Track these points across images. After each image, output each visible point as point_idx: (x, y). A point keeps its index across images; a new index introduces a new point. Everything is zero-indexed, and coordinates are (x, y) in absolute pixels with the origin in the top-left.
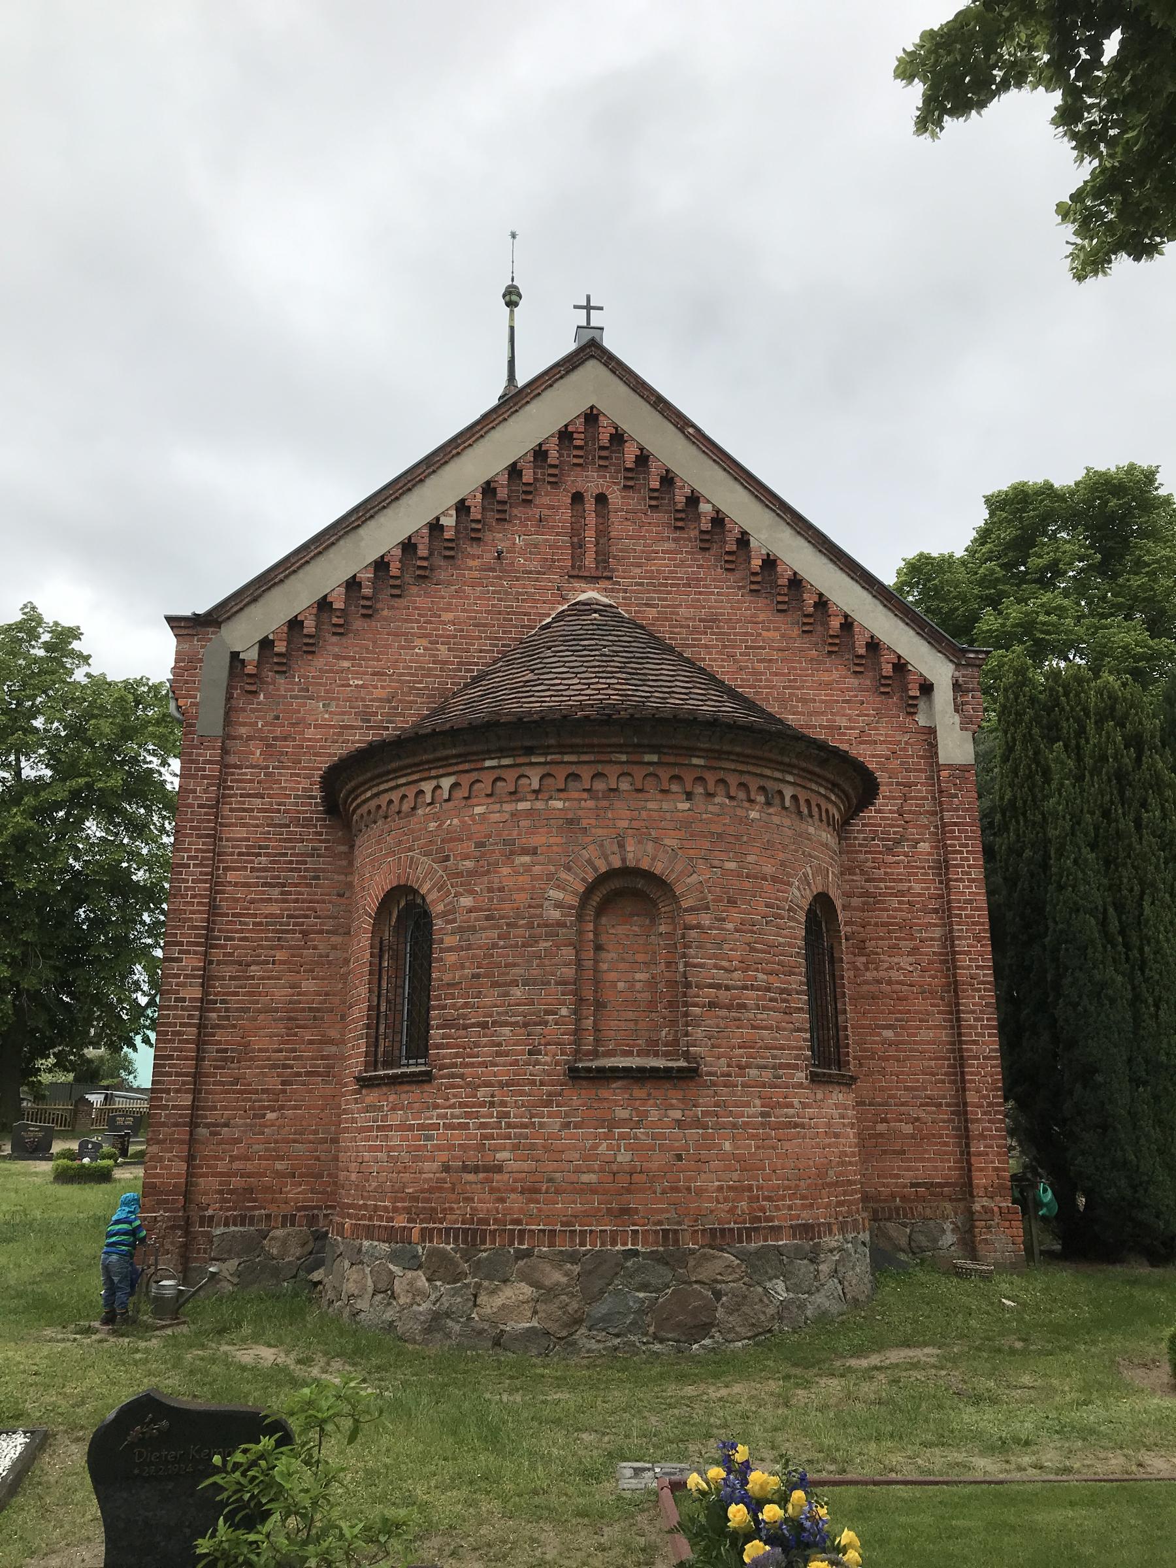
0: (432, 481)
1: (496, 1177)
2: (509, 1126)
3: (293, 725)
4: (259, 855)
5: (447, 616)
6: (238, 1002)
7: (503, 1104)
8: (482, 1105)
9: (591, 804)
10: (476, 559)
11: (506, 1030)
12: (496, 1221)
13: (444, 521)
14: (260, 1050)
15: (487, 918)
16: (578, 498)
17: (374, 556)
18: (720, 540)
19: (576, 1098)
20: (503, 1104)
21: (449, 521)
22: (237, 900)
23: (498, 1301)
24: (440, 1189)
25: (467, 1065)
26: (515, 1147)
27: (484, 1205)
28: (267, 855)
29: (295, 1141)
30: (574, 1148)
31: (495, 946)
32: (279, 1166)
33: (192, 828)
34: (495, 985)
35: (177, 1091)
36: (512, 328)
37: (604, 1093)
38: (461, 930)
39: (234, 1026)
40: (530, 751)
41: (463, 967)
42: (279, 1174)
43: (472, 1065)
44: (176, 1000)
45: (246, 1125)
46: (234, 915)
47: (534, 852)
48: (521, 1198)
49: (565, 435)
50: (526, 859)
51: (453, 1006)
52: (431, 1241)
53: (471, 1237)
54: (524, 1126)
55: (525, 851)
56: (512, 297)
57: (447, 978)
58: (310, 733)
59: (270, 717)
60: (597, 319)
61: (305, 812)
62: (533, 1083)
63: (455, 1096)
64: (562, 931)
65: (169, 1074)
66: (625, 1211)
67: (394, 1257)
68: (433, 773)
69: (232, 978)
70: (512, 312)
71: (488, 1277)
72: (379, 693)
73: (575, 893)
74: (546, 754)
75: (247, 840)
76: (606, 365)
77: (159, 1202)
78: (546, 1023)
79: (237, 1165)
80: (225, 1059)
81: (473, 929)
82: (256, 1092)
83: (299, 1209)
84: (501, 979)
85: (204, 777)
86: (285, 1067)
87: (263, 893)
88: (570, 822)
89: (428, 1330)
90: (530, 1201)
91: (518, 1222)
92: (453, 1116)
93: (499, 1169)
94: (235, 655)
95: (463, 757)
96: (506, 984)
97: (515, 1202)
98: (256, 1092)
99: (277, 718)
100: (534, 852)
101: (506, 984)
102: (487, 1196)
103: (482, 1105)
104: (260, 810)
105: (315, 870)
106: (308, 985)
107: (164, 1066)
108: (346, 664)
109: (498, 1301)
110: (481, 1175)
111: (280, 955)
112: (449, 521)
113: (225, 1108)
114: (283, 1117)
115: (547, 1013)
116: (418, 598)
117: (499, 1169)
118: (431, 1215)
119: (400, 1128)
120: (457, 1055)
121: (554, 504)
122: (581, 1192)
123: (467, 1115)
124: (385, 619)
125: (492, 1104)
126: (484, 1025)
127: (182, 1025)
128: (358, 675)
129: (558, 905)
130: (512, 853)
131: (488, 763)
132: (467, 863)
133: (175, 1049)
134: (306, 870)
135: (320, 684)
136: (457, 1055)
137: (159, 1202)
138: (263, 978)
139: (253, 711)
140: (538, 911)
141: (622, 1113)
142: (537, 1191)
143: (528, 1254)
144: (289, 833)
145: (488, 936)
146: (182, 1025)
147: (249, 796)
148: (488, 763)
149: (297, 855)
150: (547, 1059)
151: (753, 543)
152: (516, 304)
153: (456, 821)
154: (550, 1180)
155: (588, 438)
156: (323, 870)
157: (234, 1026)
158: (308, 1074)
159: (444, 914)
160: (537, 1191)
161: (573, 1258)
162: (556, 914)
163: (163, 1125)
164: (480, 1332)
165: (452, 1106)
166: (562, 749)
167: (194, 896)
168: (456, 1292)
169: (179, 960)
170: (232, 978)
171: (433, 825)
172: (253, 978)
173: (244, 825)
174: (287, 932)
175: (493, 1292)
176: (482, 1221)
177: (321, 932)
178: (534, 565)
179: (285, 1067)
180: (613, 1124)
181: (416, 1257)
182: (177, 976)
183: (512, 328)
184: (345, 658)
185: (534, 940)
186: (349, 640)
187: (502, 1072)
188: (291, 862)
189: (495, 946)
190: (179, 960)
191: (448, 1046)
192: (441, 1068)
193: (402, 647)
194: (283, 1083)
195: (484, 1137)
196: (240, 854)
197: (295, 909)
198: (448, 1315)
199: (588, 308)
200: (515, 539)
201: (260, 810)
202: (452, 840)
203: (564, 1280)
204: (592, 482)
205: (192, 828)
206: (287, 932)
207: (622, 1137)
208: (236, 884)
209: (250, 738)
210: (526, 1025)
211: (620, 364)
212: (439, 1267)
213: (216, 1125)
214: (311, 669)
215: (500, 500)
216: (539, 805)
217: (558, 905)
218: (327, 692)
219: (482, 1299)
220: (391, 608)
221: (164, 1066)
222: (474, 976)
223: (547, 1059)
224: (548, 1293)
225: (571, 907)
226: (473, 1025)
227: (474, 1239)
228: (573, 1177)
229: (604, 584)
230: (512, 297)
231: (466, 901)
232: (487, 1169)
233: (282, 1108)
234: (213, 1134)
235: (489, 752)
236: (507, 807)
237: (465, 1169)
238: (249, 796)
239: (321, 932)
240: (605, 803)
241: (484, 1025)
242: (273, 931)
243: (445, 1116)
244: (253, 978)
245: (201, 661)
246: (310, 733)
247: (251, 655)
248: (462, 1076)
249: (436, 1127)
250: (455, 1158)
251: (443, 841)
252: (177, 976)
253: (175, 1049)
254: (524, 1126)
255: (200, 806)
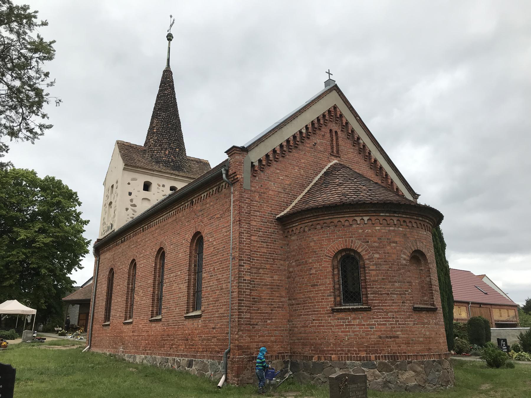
0: (299, 117)
1: (397, 339)
2: (399, 324)
3: (266, 189)
4: (259, 231)
5: (303, 161)
6: (257, 282)
7: (397, 318)
8: (390, 318)
9: (408, 230)
10: (308, 144)
11: (395, 296)
12: (399, 353)
13: (303, 131)
14: (264, 299)
15: (385, 261)
16: (331, 130)
17: (286, 138)
18: (363, 150)
19: (415, 316)
20: (397, 318)
21: (304, 131)
22: (255, 246)
23: (405, 377)
24: (378, 344)
25: (383, 306)
26: (402, 331)
27: (394, 348)
28: (262, 232)
29: (276, 330)
30: (416, 331)
31: (388, 270)
32: (273, 339)
33: (244, 220)
34: (390, 282)
35: (246, 312)
36: (169, 48)
37: (421, 315)
38: (376, 264)
39: (256, 290)
40: (395, 212)
41: (378, 276)
42: (272, 342)
43: (385, 306)
44: (244, 280)
45: (262, 325)
46: (254, 251)
47: (396, 243)
48: (405, 346)
49: (329, 111)
50: (394, 245)
51: (376, 288)
52: (379, 359)
53: (394, 357)
54: (403, 324)
55: (394, 242)
56: (170, 37)
57: (372, 279)
58: (271, 192)
59: (260, 185)
60: (332, 77)
61: (271, 219)
62: (404, 312)
63: (380, 315)
64: (406, 267)
65: (243, 306)
66: (430, 349)
67: (364, 365)
68: (361, 215)
69: (255, 273)
70: (169, 43)
71: (400, 370)
72: (288, 183)
73: (408, 256)
74: (398, 214)
75: (256, 226)
76: (338, 93)
77: (243, 352)
78: (405, 294)
79: (261, 339)
80: (255, 301)
81: (381, 265)
82: (264, 313)
83: (279, 353)
84: (392, 280)
85: (246, 203)
86: (272, 305)
87: (261, 244)
88: (405, 235)
89: (383, 387)
90: (408, 346)
91: (405, 353)
92: (380, 321)
93: (398, 337)
94: (252, 163)
95: (375, 212)
96: (393, 282)
97: (403, 347)
98: (264, 313)
99: (262, 186)
100: (396, 243)
101: (393, 282)
102: (395, 345)
103: (390, 318)
104: (259, 216)
105: (275, 238)
106: (276, 277)
107: (241, 303)
108: (278, 171)
109: (405, 377)
110: (393, 339)
111: (268, 266)
112: (304, 131)
113: (256, 319)
114: (272, 322)
115: (406, 291)
116: (295, 154)
117: (398, 337)
118: (376, 352)
119: (357, 325)
120: (379, 303)
121: (325, 130)
122: (420, 344)
123: (385, 321)
124: (288, 159)
125: (393, 318)
126: (388, 294)
127: (246, 289)
128: (282, 175)
129: (405, 259)
130: (390, 242)
131: (382, 214)
132: (376, 244)
133: (244, 297)
134: (272, 238)
135: (272, 177)
136: (379, 303)
137: (243, 352)
138: (263, 274)
139: (255, 182)
140: (399, 261)
141: (426, 321)
142: (409, 344)
143: (411, 362)
144: (267, 225)
145: (385, 267)
146: (246, 289)
147: (256, 211)
148: (382, 214)
149: (270, 233)
150: (407, 305)
151: (372, 155)
152: (171, 40)
153: (369, 231)
154: (412, 340)
155: (333, 114)
156: (277, 239)
157: (256, 290)
158: (278, 307)
159: (368, 259)
160: (409, 344)
161: (422, 363)
162: (404, 262)
163: (242, 324)
164: (401, 387)
165: (380, 318)
166: (404, 213)
167: (246, 244)
168: (392, 375)
169: (243, 266)
170: (255, 273)
171: (360, 231)
172: (260, 273)
173: (255, 221)
174: (269, 258)
175: (402, 374)
176: (394, 353)
177: (278, 259)
178: (322, 149)
179: (272, 305)
180: (424, 324)
181: (374, 365)
182: (243, 271)
183: (169, 48)
184: (278, 169)
185: (399, 269)
186: (278, 163)
187: (394, 308)
188: (268, 235)
189: (388, 270)
190: (243, 266)
191: (376, 300)
192: (374, 306)
193: (292, 169)
194: (272, 310)
195: (392, 328)
196: (255, 231)
197: (271, 251)
198: (389, 382)
199: (329, 74)
200: (316, 139)
201: (259, 216)
202: (368, 236)
203: (421, 369)
204: (335, 127)
205: (244, 220)
206: (269, 258)
207: (427, 327)
208: (254, 241)
209: (255, 192)
210: (400, 294)
211: (342, 93)
212: (383, 368)
213: (254, 325)
214: (269, 171)
215: (315, 127)
216: (396, 229)
217: (405, 259)
218: (274, 179)
219: (400, 376)
220: (289, 155)
221: (241, 303)
222: (382, 279)
223: (407, 305)
224: (418, 373)
225: (408, 260)
226: (384, 294)
227: (395, 358)
228: (417, 339)
229: (338, 159)
230: (170, 37)
231: (377, 256)
232: (394, 337)
233: (271, 319)
234: (253, 328)
235: (383, 211)
236: (386, 228)
237: (387, 337)
238: (256, 211)
239: (278, 259)
240: (412, 230)
241: (388, 294)
242: (266, 258)
243: (378, 321)
244: (260, 273)
245: (243, 163)
246: (271, 192)
247: (256, 164)
248: (382, 309)
249: (375, 325)
250: (382, 334)
251: (365, 236)
252: (243, 271)
253: (244, 297)
254: (403, 324)
255: (246, 213)
